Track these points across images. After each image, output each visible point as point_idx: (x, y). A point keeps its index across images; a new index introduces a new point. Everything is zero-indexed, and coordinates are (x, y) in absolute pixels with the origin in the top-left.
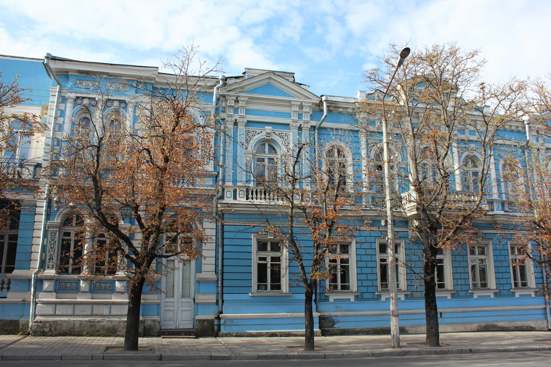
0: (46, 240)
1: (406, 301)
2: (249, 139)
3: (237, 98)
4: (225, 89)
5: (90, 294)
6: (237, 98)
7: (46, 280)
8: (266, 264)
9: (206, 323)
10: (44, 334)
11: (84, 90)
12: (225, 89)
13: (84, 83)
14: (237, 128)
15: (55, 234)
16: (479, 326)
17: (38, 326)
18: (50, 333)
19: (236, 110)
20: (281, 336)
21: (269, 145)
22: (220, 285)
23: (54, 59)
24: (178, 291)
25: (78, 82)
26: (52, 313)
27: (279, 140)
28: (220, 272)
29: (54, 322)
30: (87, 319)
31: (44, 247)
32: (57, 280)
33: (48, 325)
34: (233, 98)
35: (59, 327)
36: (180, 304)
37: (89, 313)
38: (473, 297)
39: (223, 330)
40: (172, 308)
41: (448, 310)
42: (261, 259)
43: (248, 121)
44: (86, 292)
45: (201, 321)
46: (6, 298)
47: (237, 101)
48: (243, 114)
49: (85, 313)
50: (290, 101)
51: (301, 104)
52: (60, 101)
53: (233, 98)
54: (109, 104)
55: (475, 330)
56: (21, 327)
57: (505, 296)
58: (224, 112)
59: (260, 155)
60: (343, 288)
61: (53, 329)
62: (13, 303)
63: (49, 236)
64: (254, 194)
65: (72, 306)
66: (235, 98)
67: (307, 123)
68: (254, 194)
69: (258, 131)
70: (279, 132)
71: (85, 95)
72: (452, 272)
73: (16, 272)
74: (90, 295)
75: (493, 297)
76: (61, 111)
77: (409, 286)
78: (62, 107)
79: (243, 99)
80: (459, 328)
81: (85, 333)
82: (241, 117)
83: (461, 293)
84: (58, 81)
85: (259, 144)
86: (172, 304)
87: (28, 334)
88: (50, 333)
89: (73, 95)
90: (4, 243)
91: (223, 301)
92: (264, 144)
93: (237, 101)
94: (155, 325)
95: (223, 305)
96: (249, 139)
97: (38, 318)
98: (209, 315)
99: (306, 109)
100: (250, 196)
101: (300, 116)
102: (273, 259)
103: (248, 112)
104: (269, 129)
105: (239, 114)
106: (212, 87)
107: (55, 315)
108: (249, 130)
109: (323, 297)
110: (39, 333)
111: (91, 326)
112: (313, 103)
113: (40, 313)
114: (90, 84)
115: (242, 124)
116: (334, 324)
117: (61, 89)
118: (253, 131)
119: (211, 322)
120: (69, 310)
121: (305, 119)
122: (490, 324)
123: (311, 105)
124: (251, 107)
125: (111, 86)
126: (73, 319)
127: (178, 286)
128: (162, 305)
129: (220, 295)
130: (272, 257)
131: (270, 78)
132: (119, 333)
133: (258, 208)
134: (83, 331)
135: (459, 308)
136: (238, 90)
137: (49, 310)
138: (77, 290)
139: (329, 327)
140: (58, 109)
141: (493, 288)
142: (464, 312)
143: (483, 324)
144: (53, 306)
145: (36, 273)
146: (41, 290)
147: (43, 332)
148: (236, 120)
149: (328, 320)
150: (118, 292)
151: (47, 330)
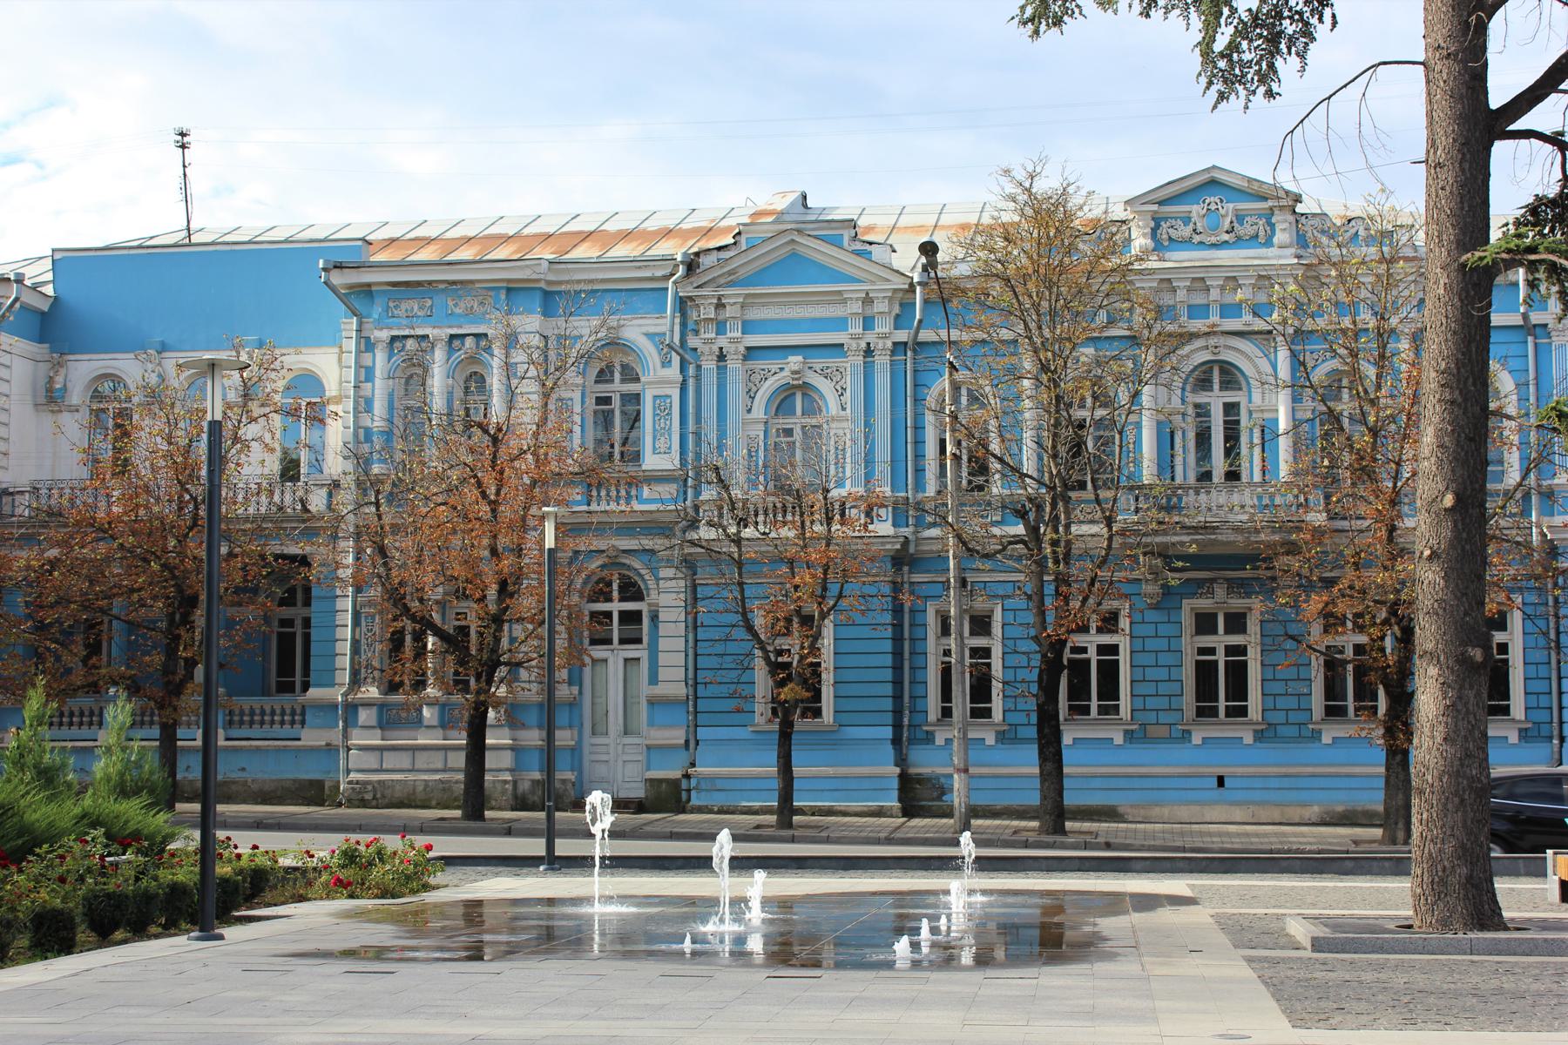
0: (358, 630)
1: (1128, 745)
2: (754, 389)
3: (719, 299)
4: (691, 283)
5: (379, 731)
6: (719, 299)
7: (362, 705)
8: (1088, 661)
9: (664, 785)
10: (363, 804)
11: (405, 322)
12: (691, 283)
13: (404, 306)
15: (373, 617)
16: (1327, 813)
17: (353, 789)
18: (374, 803)
19: (721, 327)
20: (813, 814)
21: (804, 394)
22: (691, 709)
23: (339, 266)
24: (615, 721)
25: (391, 304)
26: (376, 766)
27: (824, 386)
28: (690, 682)
29: (379, 782)
30: (437, 777)
31: (356, 644)
32: (443, 706)
33: (370, 787)
35: (388, 792)
36: (620, 747)
37: (440, 765)
38: (1320, 740)
39: (695, 801)
40: (604, 758)
41: (1240, 770)
42: (1202, 651)
43: (748, 349)
44: (434, 727)
45: (652, 782)
46: (299, 739)
47: (720, 306)
49: (432, 766)
50: (840, 292)
52: (363, 347)
54: (456, 343)
55: (1314, 820)
56: (327, 791)
57: (1156, 740)
58: (696, 332)
60: (1231, 712)
61: (379, 796)
62: (313, 749)
63: (363, 624)
65: (410, 753)
66: (715, 301)
67: (885, 337)
69: (774, 368)
70: (821, 366)
71: (406, 332)
72: (1259, 678)
73: (313, 692)
74: (440, 732)
75: (993, 743)
76: (367, 368)
77: (1009, 710)
78: (367, 359)
79: (732, 301)
80: (1264, 815)
81: (434, 803)
82: (733, 341)
83: (1282, 730)
85: (779, 394)
86: (603, 749)
87: (340, 805)
88: (374, 803)
89: (385, 335)
90: (295, 633)
91: (697, 743)
92: (1211, 369)
93: (720, 306)
94: (566, 790)
95: (1561, 746)
96: (754, 389)
97: (353, 776)
98: (670, 771)
99: (880, 306)
101: (868, 323)
102: (1230, 650)
103: (748, 327)
104: (795, 361)
105: (729, 335)
106: (667, 278)
107: (380, 770)
109: (920, 735)
110: (357, 803)
111: (444, 789)
112: (895, 291)
113: (356, 767)
114: (416, 308)
116: (943, 793)
117: (360, 324)
119: (674, 784)
120: (404, 760)
122: (1360, 809)
124: (754, 314)
125: (456, 305)
126: (411, 777)
127: (617, 712)
128: (586, 750)
129: (691, 729)
130: (1098, 646)
131: (793, 240)
132: (493, 803)
134: (430, 800)
135: (1208, 766)
137: (371, 760)
138: (418, 722)
139: (933, 800)
140: (359, 366)
141: (1518, 718)
142: (1286, 776)
143: (1340, 808)
144: (378, 753)
145: (345, 695)
146: (355, 725)
147: (363, 800)
148: (721, 349)
149: (930, 785)
150: (427, 727)
151: (368, 797)
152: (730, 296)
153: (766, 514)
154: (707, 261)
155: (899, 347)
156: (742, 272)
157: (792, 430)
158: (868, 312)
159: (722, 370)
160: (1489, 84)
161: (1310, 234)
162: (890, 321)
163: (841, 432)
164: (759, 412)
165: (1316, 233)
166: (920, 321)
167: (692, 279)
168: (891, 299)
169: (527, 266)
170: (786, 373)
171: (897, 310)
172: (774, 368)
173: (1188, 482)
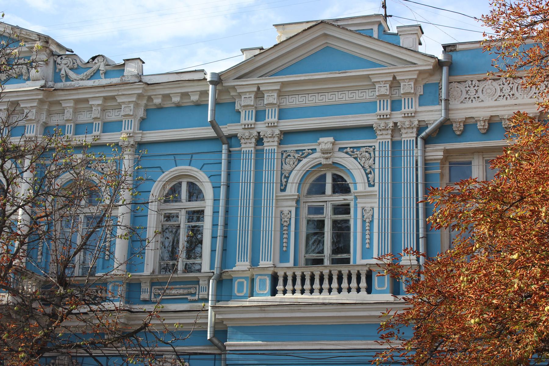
6: (394, 78)
19: (260, 115)
27: (348, 162)
50: (367, 77)
51: (259, 88)
64: (326, 282)
66: (255, 89)
68: (308, 282)
82: (272, 126)
84: (161, 84)
99: (406, 87)
100: (280, 287)
103: (282, 114)
104: (326, 141)
112: (421, 72)
121: (382, 111)
123: (134, 99)
131: (325, 35)
133: (117, 350)
153: (349, 281)
158: (396, 97)
159: (259, 154)
161: (63, 72)
162: (135, 123)
163: (368, 206)
164: (292, 190)
165: (68, 70)
168: (416, 81)
171: (420, 91)
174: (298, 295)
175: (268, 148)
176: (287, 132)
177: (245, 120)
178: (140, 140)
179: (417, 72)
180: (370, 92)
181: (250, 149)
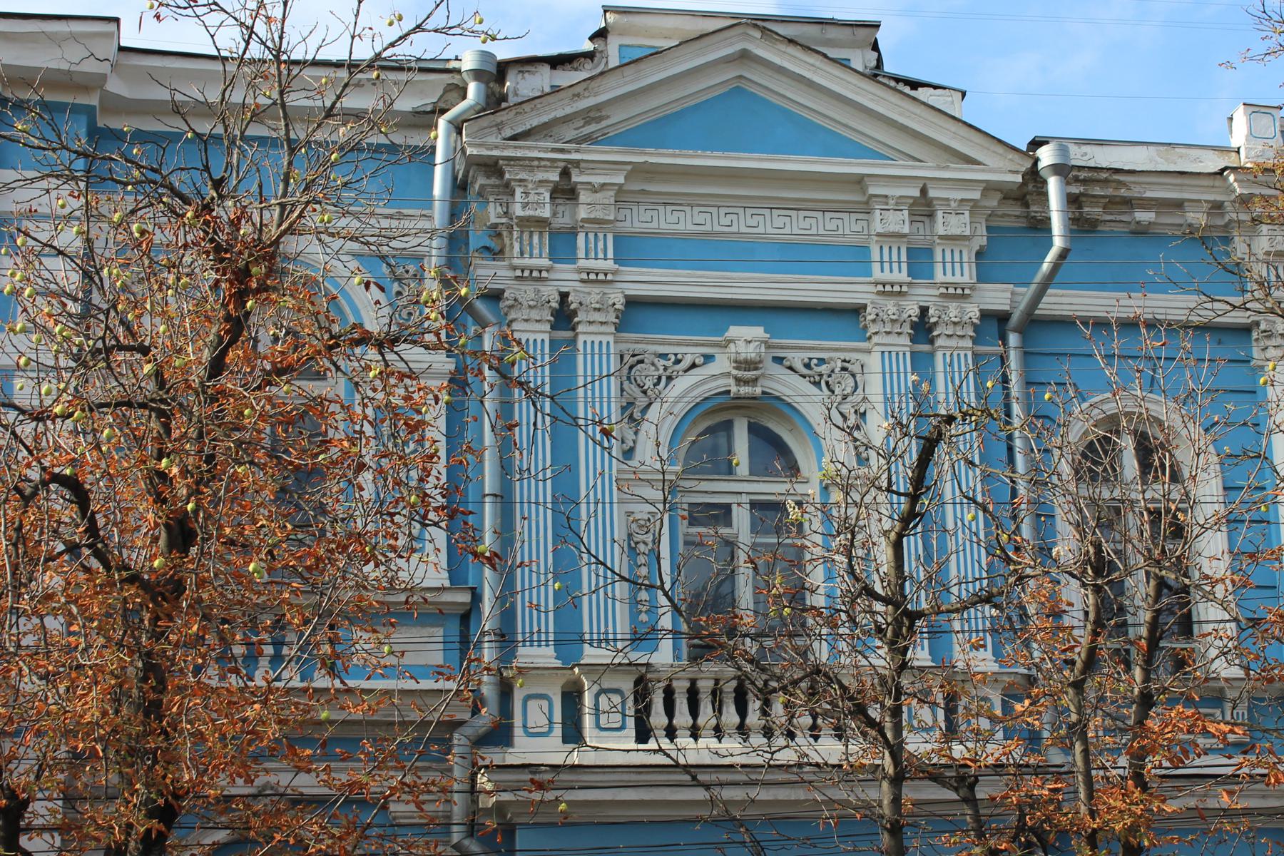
2: (642, 401)
3: (565, 173)
4: (499, 127)
6: (565, 173)
12: (499, 127)
14: (573, 341)
21: (757, 431)
34: (541, 175)
43: (633, 303)
47: (565, 192)
48: (601, 264)
51: (924, 191)
53: (541, 175)
59: (704, 486)
64: (682, 705)
66: (554, 176)
67: (959, 294)
68: (682, 705)
69: (691, 354)
70: (806, 355)
79: (597, 180)
82: (594, 279)
93: (565, 192)
99: (950, 224)
100: (658, 719)
101: (920, 260)
108: (639, 347)
112: (989, 188)
115: (534, 314)
118: (664, 356)
123: (976, 195)
124: (641, 220)
131: (744, 56)
136: (570, 133)
152: (594, 165)
154: (519, 86)
155: (996, 321)
156: (617, 116)
157: (727, 508)
160: (747, 445)
166: (1063, 255)
167: (501, 117)
169: (74, 37)
170: (722, 364)
172: (691, 354)
173: (482, 797)
174: (731, 745)
175: (589, 339)
176: (1056, 318)
177: (945, 274)
178: (1184, 318)
179: (984, 185)
180: (801, 218)
181: (539, 337)
